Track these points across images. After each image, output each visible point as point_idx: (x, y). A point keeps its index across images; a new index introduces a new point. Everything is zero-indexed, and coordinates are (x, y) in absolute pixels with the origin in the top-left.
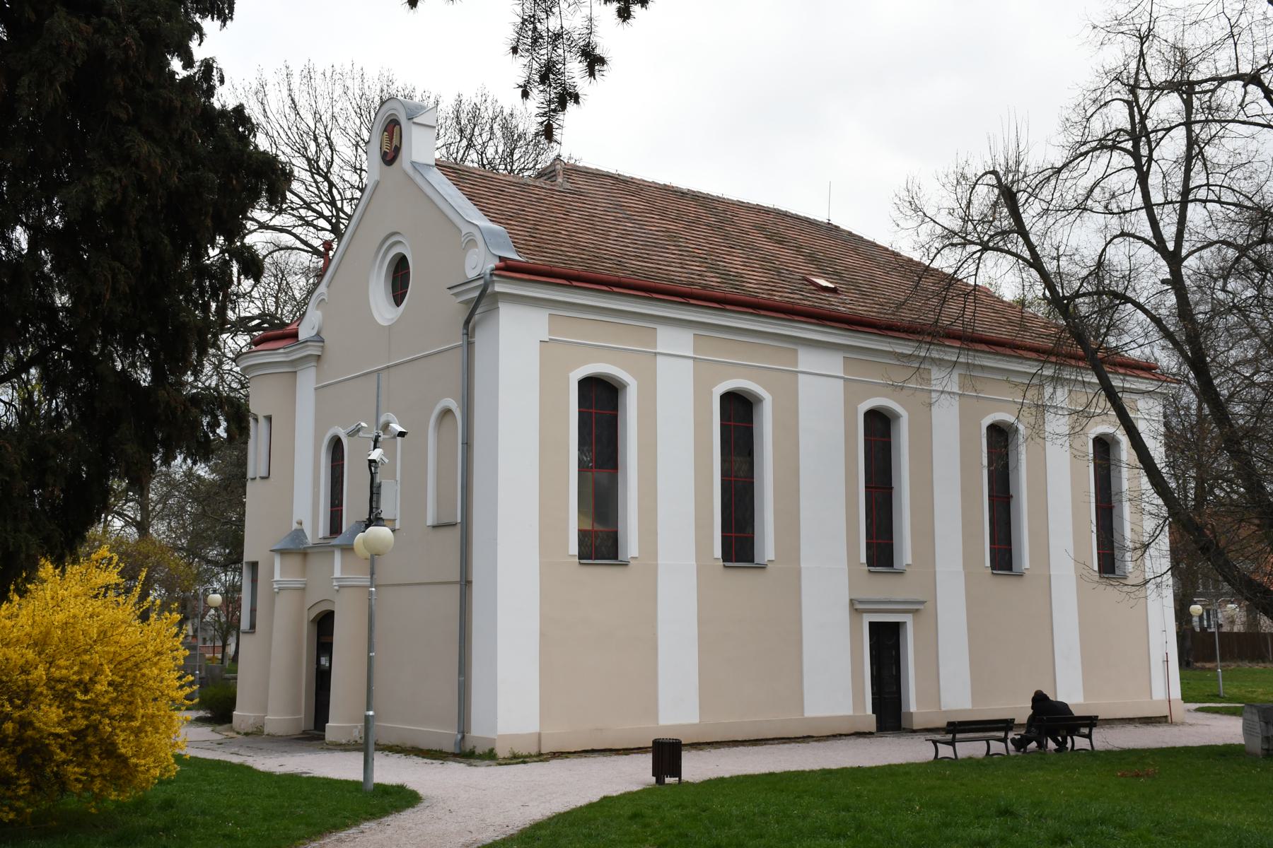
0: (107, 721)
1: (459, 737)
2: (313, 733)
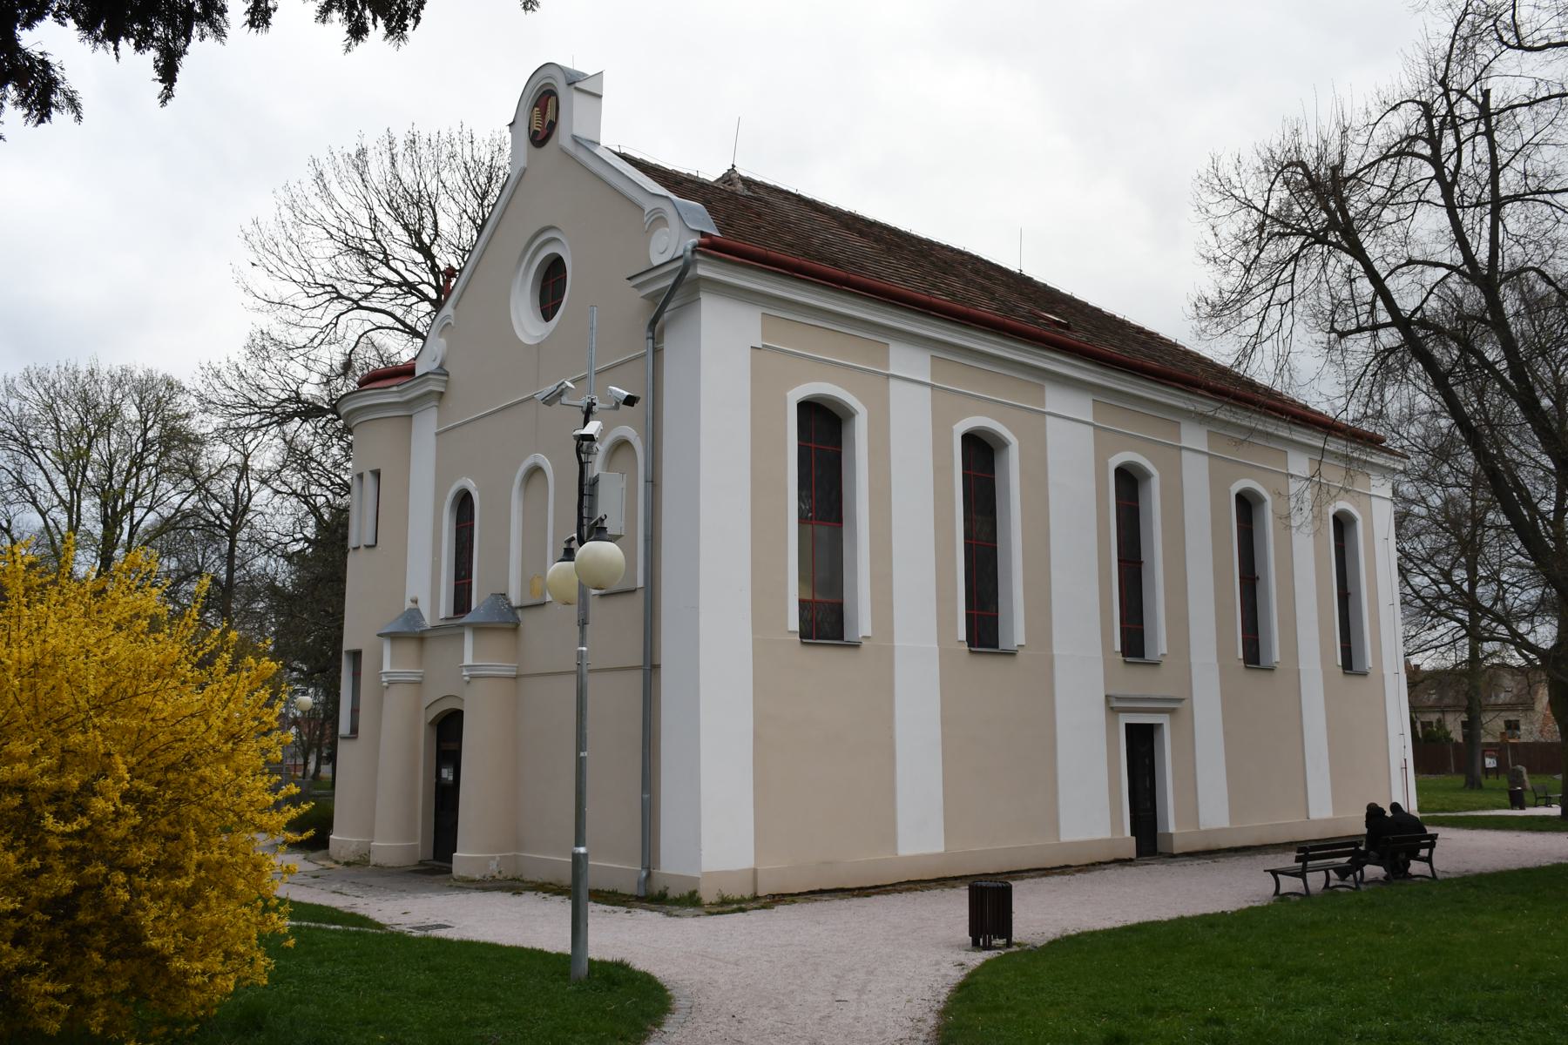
0: (121, 878)
1: (644, 874)
2: (436, 862)
